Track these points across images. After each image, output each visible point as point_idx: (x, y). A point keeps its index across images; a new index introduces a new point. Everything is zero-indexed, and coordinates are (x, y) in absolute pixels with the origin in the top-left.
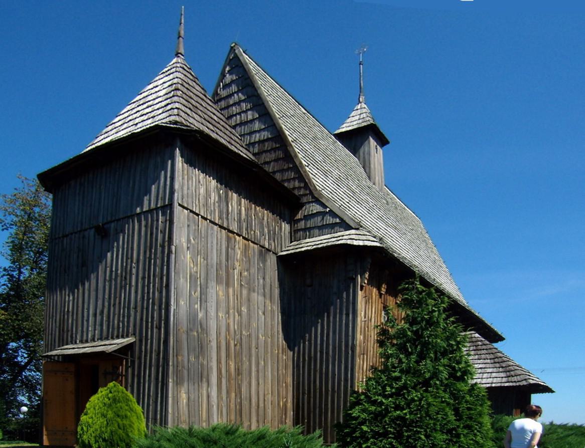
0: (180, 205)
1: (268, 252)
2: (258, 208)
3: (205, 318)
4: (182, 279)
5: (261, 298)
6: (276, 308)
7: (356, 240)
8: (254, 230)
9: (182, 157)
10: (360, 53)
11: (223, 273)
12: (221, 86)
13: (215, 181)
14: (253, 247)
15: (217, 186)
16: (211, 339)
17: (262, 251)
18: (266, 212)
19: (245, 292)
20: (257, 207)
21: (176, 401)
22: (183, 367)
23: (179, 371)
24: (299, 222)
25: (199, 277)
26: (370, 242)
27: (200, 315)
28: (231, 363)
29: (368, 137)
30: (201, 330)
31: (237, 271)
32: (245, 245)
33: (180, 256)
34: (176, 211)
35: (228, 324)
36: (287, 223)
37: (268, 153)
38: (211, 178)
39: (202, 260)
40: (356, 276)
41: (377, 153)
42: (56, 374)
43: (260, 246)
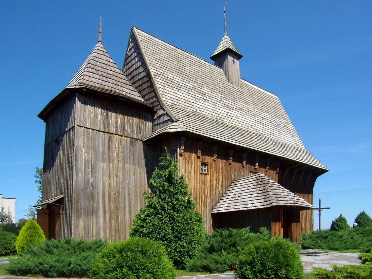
0: (78, 126)
1: (136, 140)
2: (129, 118)
3: (95, 181)
4: (80, 163)
5: (132, 167)
6: (143, 171)
7: (173, 129)
8: (126, 130)
9: (80, 101)
10: (224, 6)
11: (106, 156)
12: (129, 50)
13: (100, 109)
14: (126, 139)
15: (101, 111)
16: (99, 192)
17: (132, 140)
18: (134, 118)
19: (121, 165)
20: (128, 117)
21: (77, 226)
22: (81, 208)
23: (79, 211)
24: (155, 120)
25: (90, 160)
26: (181, 129)
27: (91, 180)
28: (112, 204)
29: (227, 56)
30: (92, 188)
31: (115, 153)
32: (121, 139)
33: (79, 151)
34: (76, 129)
35: (110, 183)
36: (150, 122)
37: (145, 84)
38: (98, 108)
39: (93, 151)
40: (177, 149)
41: (234, 64)
42: (41, 215)
43: (131, 138)
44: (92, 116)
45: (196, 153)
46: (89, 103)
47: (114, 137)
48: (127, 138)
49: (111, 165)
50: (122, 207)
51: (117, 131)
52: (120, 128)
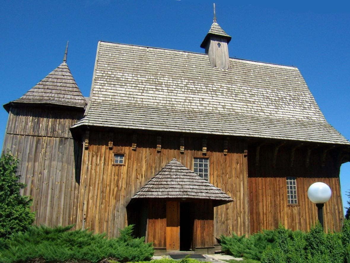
11: (32, 156)
14: (56, 139)
17: (62, 140)
44: (24, 124)
45: (107, 145)
46: (32, 114)
47: (43, 139)
48: (57, 138)
49: (37, 164)
50: (43, 201)
51: (47, 133)
52: (50, 130)
